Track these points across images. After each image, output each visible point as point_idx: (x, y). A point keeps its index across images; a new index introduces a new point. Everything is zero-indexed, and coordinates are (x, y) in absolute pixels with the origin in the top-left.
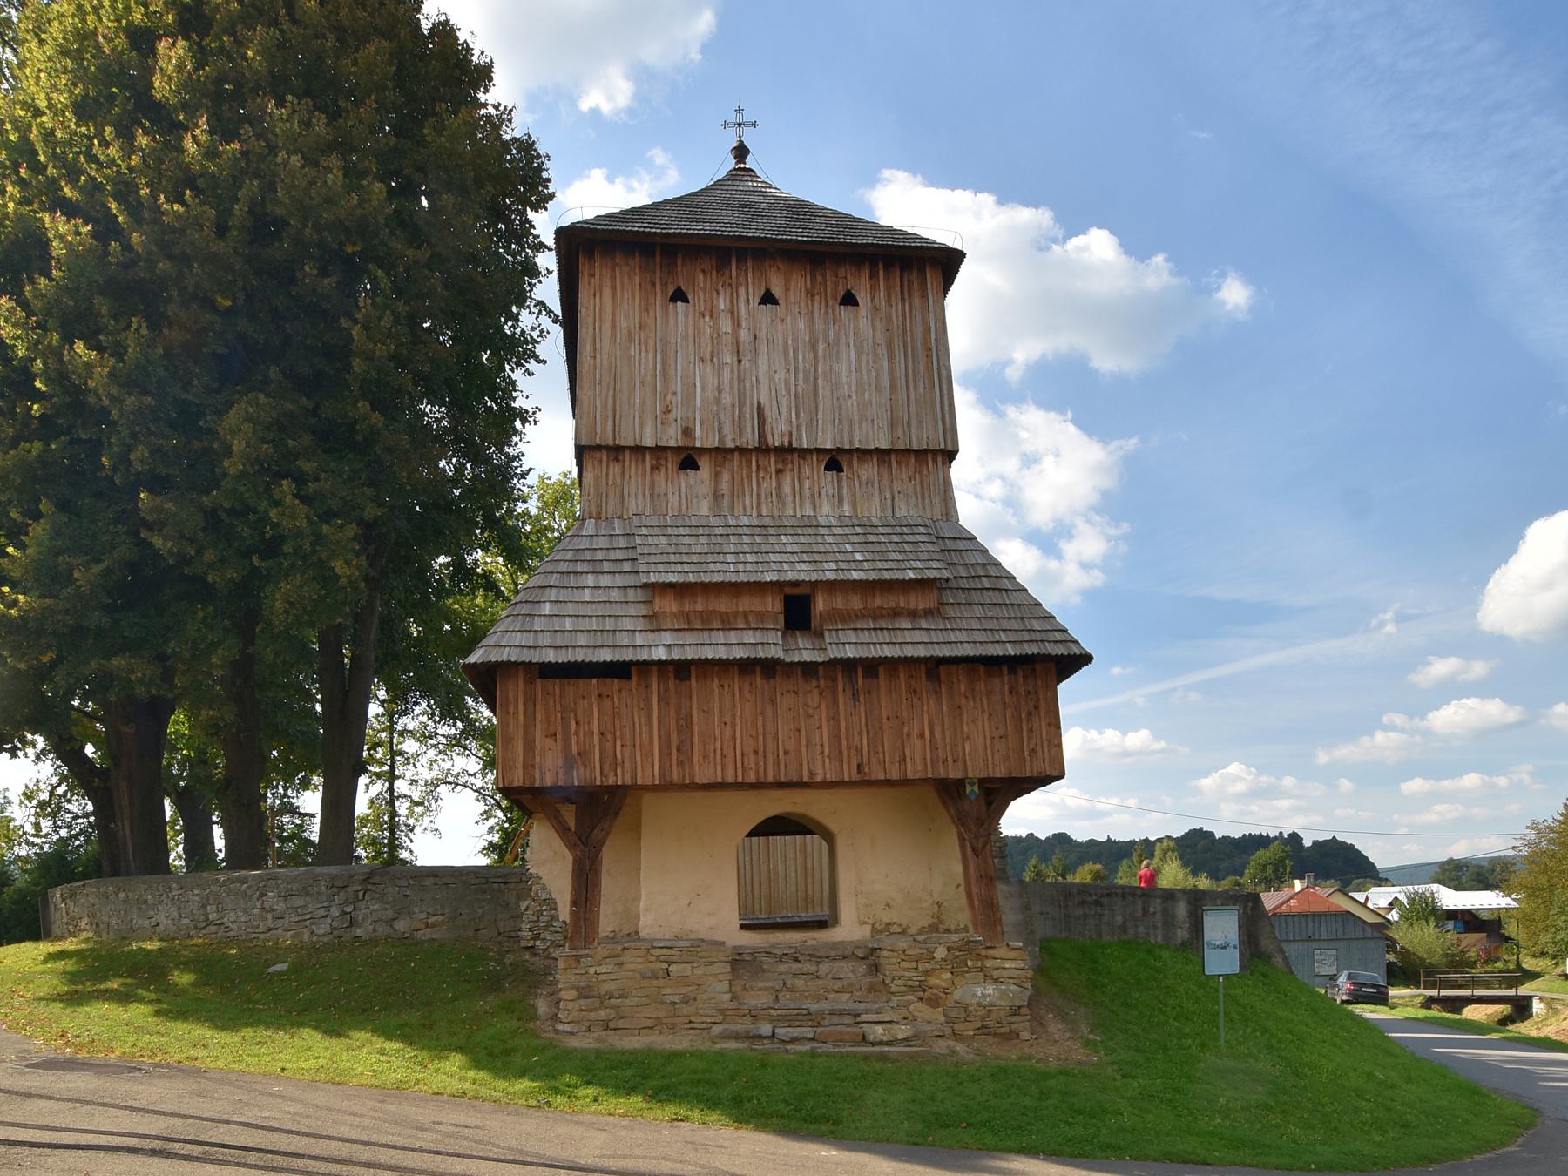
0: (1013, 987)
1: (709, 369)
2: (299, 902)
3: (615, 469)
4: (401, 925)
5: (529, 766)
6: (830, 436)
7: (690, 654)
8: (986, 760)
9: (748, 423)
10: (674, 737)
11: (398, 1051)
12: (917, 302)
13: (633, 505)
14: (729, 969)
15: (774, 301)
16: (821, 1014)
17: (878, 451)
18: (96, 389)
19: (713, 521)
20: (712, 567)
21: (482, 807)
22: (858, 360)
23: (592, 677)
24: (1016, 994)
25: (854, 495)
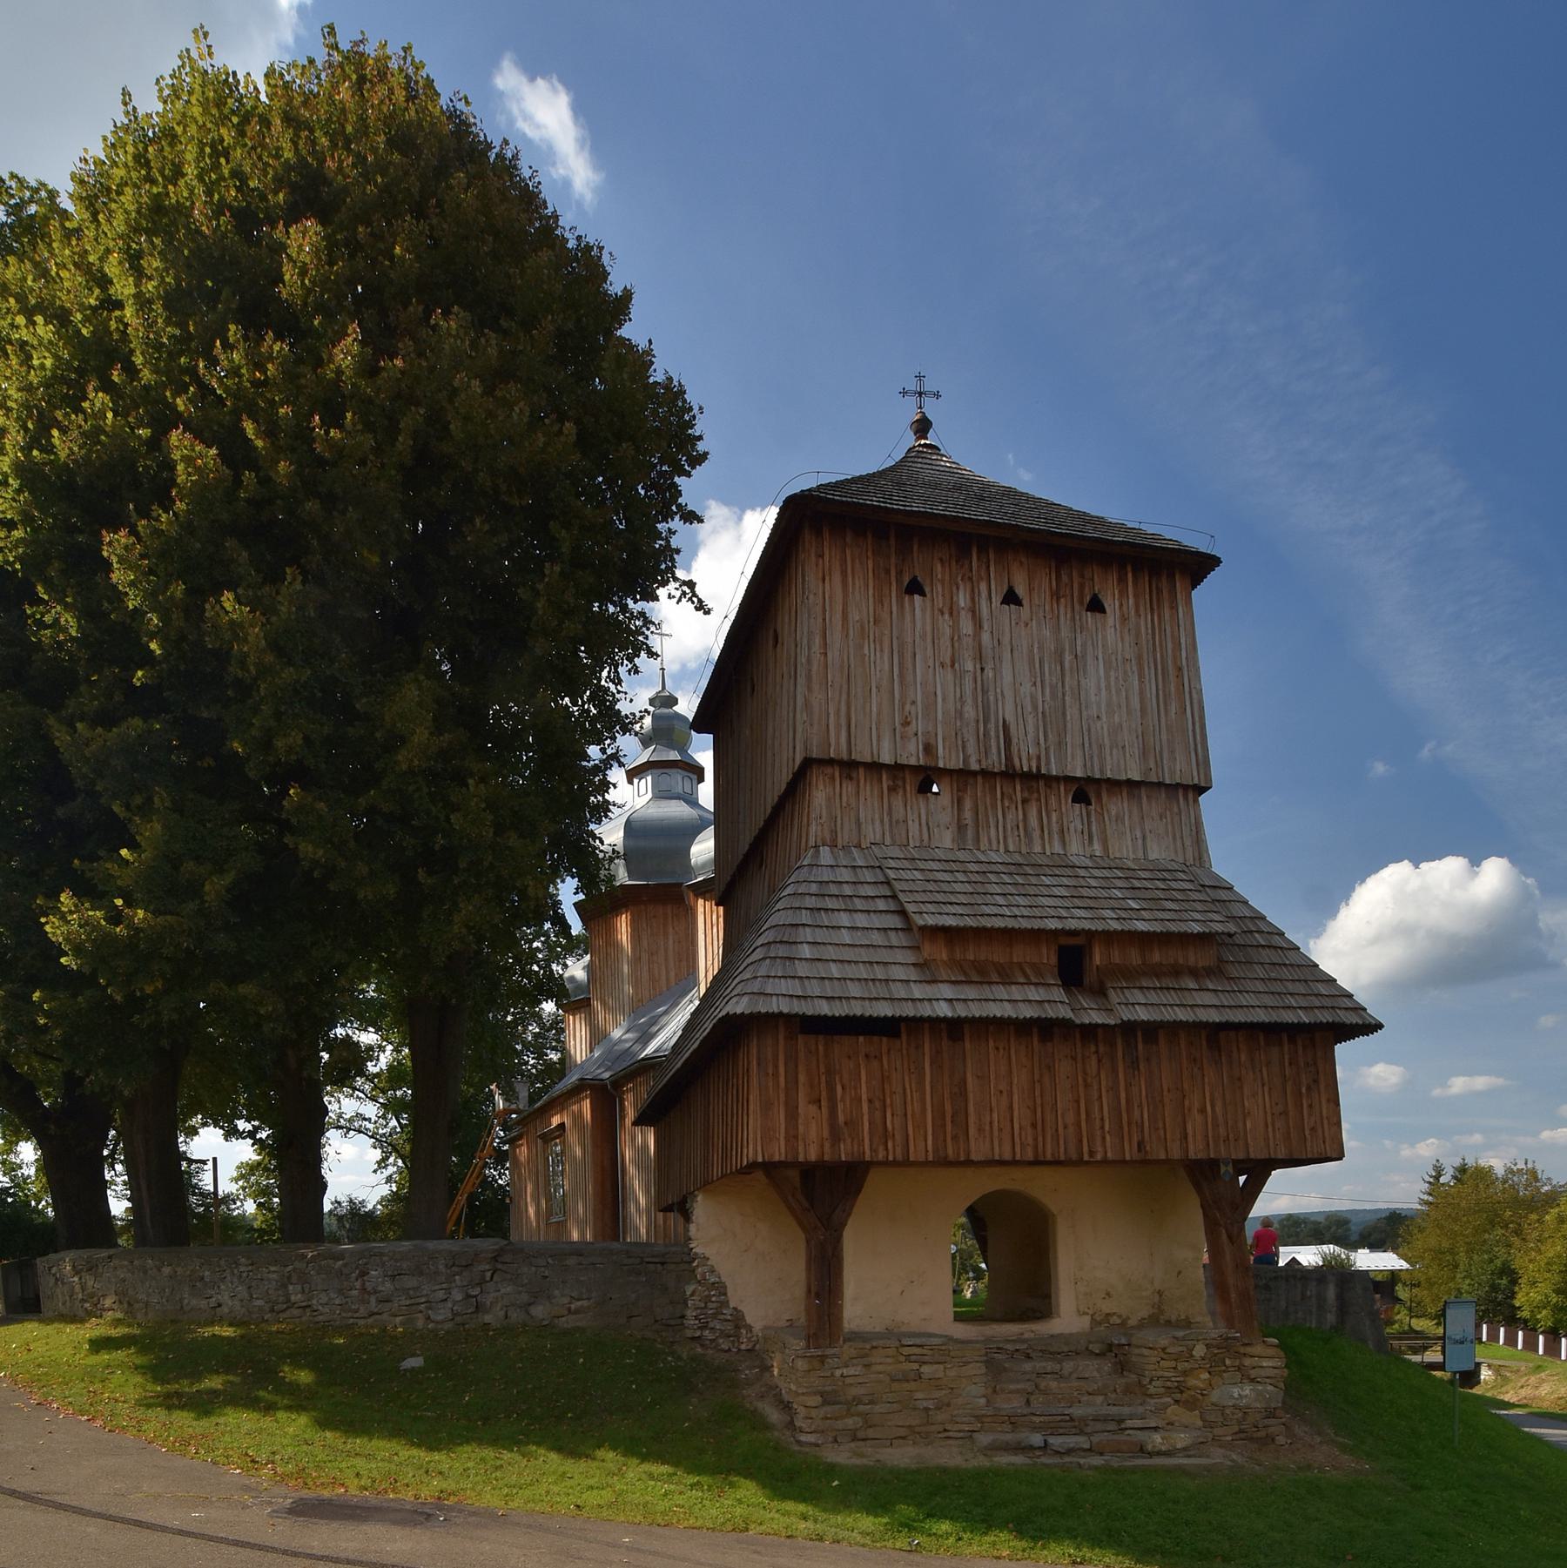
0: (1270, 1388)
1: (950, 677)
2: (410, 1282)
3: (849, 788)
4: (539, 1311)
5: (792, 1137)
6: (1079, 762)
7: (976, 1011)
8: (1267, 1139)
9: (993, 743)
10: (948, 1107)
11: (670, 1475)
12: (1167, 613)
13: (872, 832)
14: (984, 1370)
15: (1019, 603)
16: (1083, 1419)
17: (1131, 784)
18: (246, 655)
19: (961, 855)
20: (987, 910)
21: (377, 1154)
22: (1107, 678)
23: (858, 1034)
24: (1272, 1393)
25: (1104, 831)
